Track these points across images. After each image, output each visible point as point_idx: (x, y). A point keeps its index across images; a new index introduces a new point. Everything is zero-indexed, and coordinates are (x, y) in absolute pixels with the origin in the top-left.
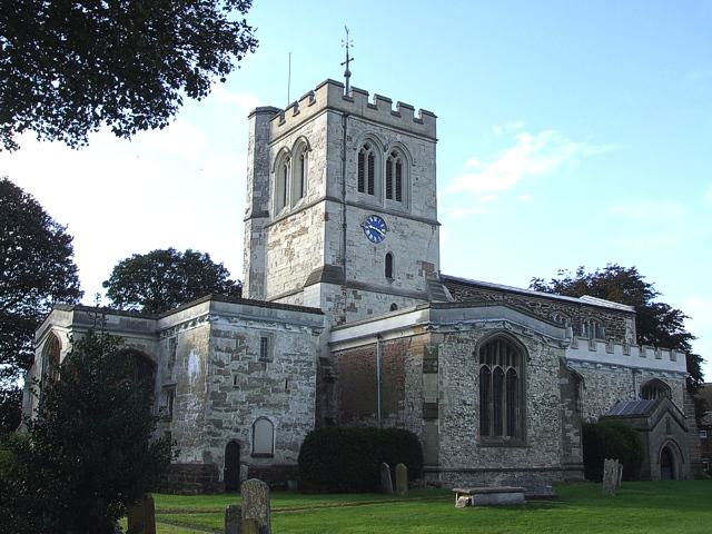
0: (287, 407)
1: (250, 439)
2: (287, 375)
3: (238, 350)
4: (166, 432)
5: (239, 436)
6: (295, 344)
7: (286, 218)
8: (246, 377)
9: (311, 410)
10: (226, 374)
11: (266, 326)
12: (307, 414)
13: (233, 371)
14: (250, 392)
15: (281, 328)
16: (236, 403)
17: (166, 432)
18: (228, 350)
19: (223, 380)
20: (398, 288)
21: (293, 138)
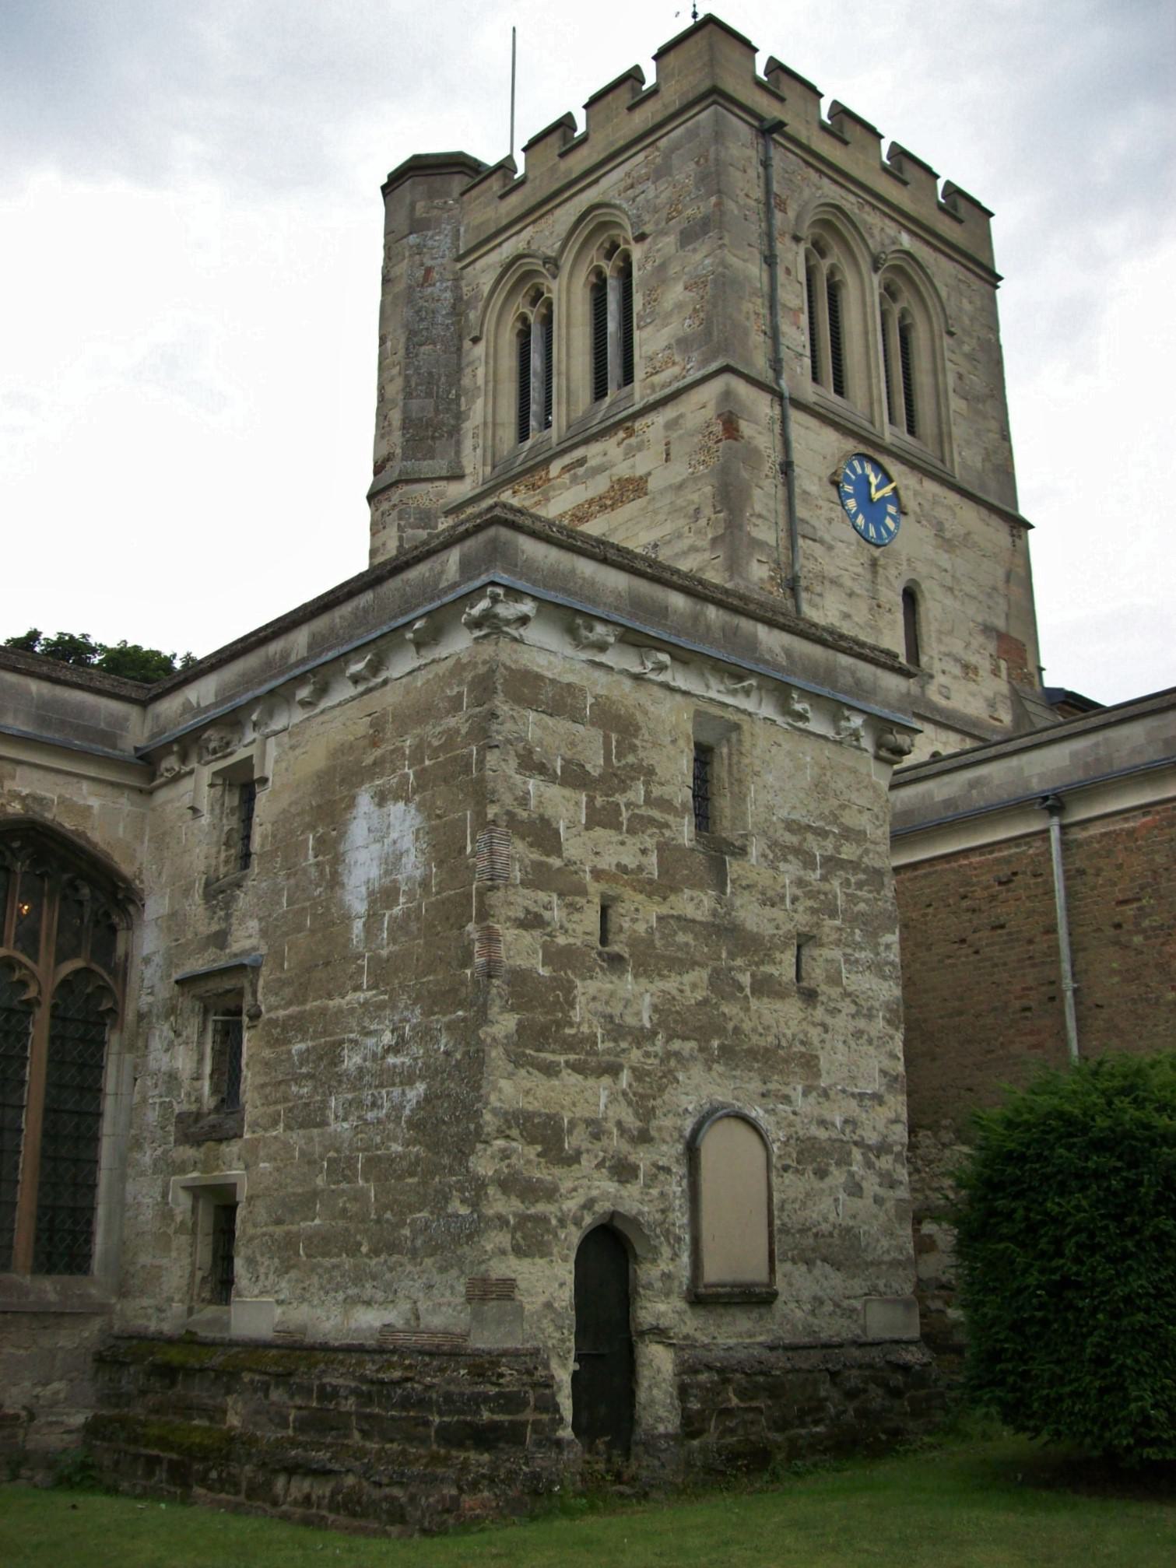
0: (809, 1063)
1: (680, 1218)
2: (802, 919)
3: (615, 780)
4: (196, 1192)
5: (632, 1199)
6: (820, 788)
7: (548, 462)
8: (653, 910)
9: (892, 1080)
10: (570, 889)
11: (715, 690)
12: (878, 1098)
13: (597, 874)
14: (671, 985)
15: (767, 710)
16: (617, 1030)
17: (196, 1192)
18: (574, 777)
19: (557, 915)
20: (943, 702)
21: (566, 215)
